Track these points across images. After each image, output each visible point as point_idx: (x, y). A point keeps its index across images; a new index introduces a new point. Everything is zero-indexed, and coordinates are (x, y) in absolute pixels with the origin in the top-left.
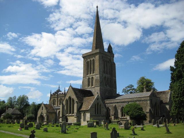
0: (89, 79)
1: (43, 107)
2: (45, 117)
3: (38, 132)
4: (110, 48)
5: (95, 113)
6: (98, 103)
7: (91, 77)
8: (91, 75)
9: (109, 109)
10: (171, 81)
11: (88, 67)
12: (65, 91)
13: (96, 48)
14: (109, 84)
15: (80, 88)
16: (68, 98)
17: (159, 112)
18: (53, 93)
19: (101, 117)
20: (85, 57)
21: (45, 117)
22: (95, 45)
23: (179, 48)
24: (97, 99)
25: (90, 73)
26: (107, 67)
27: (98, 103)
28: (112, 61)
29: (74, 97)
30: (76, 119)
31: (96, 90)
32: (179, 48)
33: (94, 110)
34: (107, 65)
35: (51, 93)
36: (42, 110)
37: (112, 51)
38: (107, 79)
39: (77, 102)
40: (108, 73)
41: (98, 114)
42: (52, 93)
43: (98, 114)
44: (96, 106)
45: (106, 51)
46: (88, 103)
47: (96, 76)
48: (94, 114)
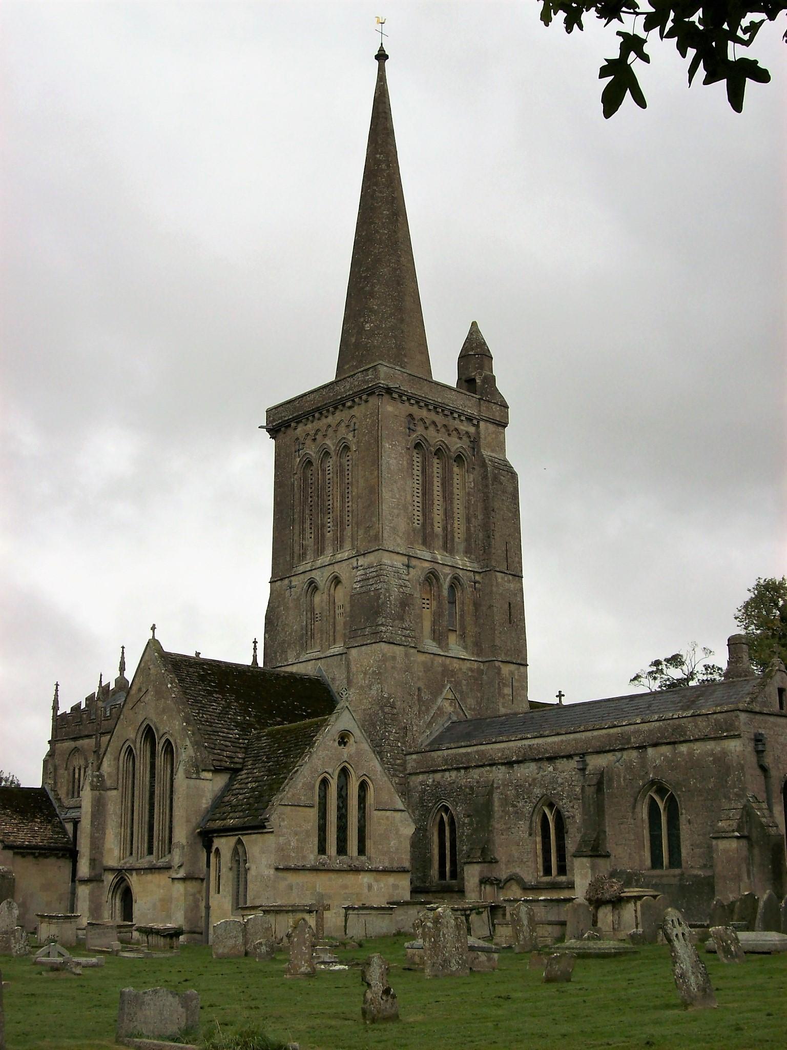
3: (782, 739)
4: (475, 355)
5: (322, 850)
6: (344, 772)
7: (327, 572)
8: (324, 559)
11: (304, 510)
12: (122, 668)
14: (463, 628)
15: (248, 662)
16: (132, 736)
17: (83, 960)
20: (283, 422)
25: (320, 551)
26: (448, 496)
27: (344, 772)
28: (486, 453)
38: (445, 593)
40: (462, 547)
41: (342, 849)
43: (342, 849)
45: (445, 369)
48: (312, 858)
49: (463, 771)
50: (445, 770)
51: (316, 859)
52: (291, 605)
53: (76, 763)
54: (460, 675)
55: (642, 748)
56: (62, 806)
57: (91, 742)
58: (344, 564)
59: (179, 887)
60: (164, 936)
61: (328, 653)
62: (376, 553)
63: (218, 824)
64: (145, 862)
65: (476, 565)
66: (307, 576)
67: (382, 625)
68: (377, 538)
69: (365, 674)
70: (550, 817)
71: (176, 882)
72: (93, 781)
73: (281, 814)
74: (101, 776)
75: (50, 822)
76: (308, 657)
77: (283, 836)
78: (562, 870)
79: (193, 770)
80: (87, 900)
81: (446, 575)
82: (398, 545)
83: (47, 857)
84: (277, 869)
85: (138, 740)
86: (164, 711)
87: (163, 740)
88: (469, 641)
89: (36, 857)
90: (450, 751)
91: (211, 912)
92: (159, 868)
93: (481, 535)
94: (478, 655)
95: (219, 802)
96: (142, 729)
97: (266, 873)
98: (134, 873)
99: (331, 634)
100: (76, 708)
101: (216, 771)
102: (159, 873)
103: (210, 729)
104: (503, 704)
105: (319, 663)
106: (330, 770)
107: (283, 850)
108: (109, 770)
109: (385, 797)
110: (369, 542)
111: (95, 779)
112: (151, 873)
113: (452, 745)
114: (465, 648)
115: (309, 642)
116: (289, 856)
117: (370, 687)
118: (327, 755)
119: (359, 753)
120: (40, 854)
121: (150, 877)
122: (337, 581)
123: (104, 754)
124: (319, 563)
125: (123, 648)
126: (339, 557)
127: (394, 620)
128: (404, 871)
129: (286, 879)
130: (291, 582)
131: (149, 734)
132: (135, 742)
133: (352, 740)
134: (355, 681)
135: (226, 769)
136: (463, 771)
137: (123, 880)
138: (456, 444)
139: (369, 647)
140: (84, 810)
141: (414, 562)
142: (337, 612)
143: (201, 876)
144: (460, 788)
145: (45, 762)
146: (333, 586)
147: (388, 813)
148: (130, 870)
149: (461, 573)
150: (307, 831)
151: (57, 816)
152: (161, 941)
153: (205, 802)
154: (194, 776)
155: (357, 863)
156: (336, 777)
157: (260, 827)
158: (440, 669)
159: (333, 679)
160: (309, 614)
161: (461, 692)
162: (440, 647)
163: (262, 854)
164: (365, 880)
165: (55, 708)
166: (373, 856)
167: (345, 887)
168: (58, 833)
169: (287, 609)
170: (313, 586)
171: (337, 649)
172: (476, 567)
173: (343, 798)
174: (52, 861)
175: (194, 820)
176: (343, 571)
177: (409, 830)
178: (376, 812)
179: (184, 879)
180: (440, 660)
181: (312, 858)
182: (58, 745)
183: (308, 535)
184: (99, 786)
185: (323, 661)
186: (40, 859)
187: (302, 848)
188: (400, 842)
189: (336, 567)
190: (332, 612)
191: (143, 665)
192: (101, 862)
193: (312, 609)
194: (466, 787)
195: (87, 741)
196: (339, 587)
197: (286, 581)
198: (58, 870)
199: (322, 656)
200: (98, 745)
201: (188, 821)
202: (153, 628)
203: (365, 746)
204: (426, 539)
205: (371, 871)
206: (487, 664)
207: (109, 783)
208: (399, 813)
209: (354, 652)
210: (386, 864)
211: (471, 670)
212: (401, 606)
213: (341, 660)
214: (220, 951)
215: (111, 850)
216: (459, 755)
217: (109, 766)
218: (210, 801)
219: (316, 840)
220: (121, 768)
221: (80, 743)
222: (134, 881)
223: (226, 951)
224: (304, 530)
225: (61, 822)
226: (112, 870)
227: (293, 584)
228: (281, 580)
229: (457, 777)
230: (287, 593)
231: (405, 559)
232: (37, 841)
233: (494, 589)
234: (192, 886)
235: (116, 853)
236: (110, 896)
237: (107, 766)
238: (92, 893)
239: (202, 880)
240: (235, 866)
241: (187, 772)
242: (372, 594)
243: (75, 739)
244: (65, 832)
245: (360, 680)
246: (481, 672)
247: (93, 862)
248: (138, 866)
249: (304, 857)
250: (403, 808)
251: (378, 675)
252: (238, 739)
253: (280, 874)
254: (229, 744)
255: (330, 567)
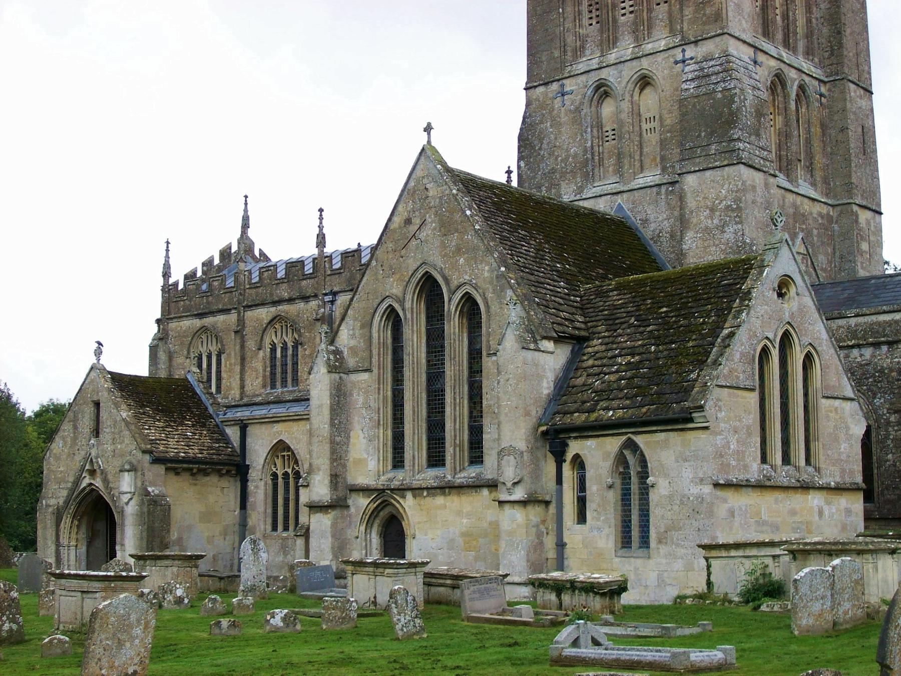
7: (629, 72)
14: (810, 157)
25: (609, 41)
27: (786, 341)
49: (885, 348)
50: (852, 347)
51: (761, 471)
52: (564, 119)
53: (204, 350)
54: (811, 222)
56: (216, 404)
57: (233, 317)
58: (660, 57)
59: (518, 515)
60: (603, 595)
61: (634, 184)
62: (718, 39)
63: (579, 418)
64: (430, 476)
65: (819, 71)
66: (593, 77)
67: (739, 139)
68: (718, 17)
69: (712, 210)
71: (507, 507)
72: (329, 359)
73: (719, 400)
74: (337, 352)
75: (204, 425)
76: (597, 191)
77: (720, 434)
79: (528, 337)
80: (329, 535)
81: (793, 80)
82: (744, 31)
83: (206, 474)
84: (716, 485)
85: (409, 297)
86: (458, 250)
87: (459, 295)
88: (818, 175)
89: (193, 475)
90: (860, 320)
91: (568, 551)
92: (461, 487)
93: (825, 30)
94: (827, 195)
95: (564, 386)
96: (415, 280)
97: (695, 490)
98: (409, 495)
99: (637, 157)
100: (190, 277)
101: (559, 340)
102: (459, 494)
103: (532, 278)
104: (862, 263)
105: (619, 199)
106: (771, 336)
107: (721, 456)
108: (353, 343)
109: (833, 380)
110: (704, 24)
111: (332, 357)
112: (444, 494)
113: (865, 311)
114: (813, 184)
115: (596, 170)
116: (729, 465)
117: (722, 228)
118: (766, 312)
119: (801, 309)
120: (199, 470)
121: (440, 500)
122: (645, 82)
123: (343, 319)
124: (612, 57)
125: (246, 197)
126: (612, 57)
127: (750, 135)
128: (858, 489)
129: (725, 501)
130: (563, 86)
131: (430, 289)
132: (402, 302)
133: (793, 290)
134: (694, 220)
135: (572, 337)
136: (885, 348)
137: (385, 504)
139: (718, 172)
140: (314, 402)
141: (761, 58)
142: (645, 126)
143: (547, 498)
144: (882, 371)
145: (153, 349)
146: (637, 89)
147: (837, 403)
148: (402, 490)
149: (807, 79)
150: (748, 427)
151: (211, 417)
152: (596, 603)
153: (547, 387)
154: (532, 346)
155: (805, 477)
156: (777, 346)
157: (681, 420)
158: (791, 211)
159: (645, 221)
160: (595, 131)
161: (813, 246)
163: (676, 464)
164: (816, 502)
165: (166, 274)
166: (822, 466)
167: (793, 513)
168: (218, 441)
169: (556, 124)
170: (602, 91)
171: (651, 176)
172: (818, 73)
174: (213, 479)
175: (534, 413)
176: (659, 68)
177: (859, 430)
178: (824, 401)
179: (524, 503)
180: (790, 197)
181: (754, 470)
182: (173, 325)
183: (585, 22)
184: (338, 366)
185: (625, 195)
186: (199, 477)
187: (743, 452)
188: (851, 446)
189: (645, 63)
190: (637, 128)
191: (412, 184)
192: (345, 479)
193: (599, 125)
194: (891, 370)
195: (221, 318)
196: (647, 90)
197: (555, 86)
198: (221, 494)
199: (626, 188)
200: (241, 322)
201: (528, 414)
202: (428, 129)
203: (808, 301)
205: (821, 488)
206: (839, 208)
207: (351, 362)
208: (849, 403)
209: (691, 181)
210: (838, 479)
211: (820, 214)
212: (756, 116)
213: (658, 193)
214: (804, 622)
215: (359, 462)
216: (879, 324)
217: (353, 336)
218: (552, 384)
219: (759, 439)
220: (375, 340)
221: (209, 321)
222: (409, 505)
223: (811, 621)
224: (580, 13)
225: (217, 426)
226: (365, 490)
227: (567, 89)
228: (546, 84)
229: (873, 356)
230: (557, 103)
231: (751, 51)
232: (194, 452)
233: (849, 105)
234: (534, 513)
235: (372, 465)
236: (363, 528)
237: (345, 338)
238: (334, 525)
239: (547, 503)
240: (618, 482)
241: (521, 339)
242: (719, 95)
243: (201, 316)
244: (226, 440)
245: (702, 218)
246: (830, 219)
247: (335, 479)
248: (416, 484)
249: (746, 467)
250: (852, 396)
251: (736, 211)
252: (568, 295)
253: (720, 493)
254: (561, 301)
255: (635, 63)
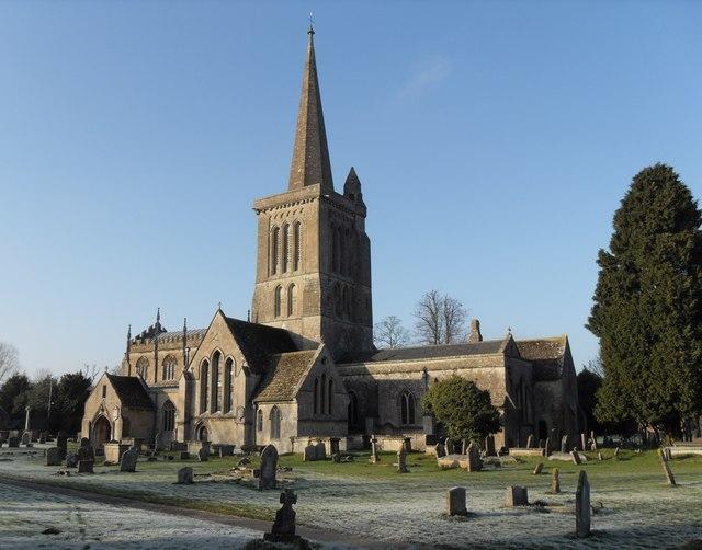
0: (278, 289)
1: (105, 387)
2: (117, 422)
6: (324, 376)
9: (278, 411)
10: (594, 299)
13: (307, 182)
18: (138, 338)
19: (331, 425)
21: (117, 422)
22: (301, 170)
23: (677, 176)
24: (322, 360)
27: (324, 376)
29: (232, 350)
30: (242, 428)
31: (307, 325)
32: (677, 176)
33: (311, 400)
34: (342, 243)
35: (129, 337)
36: (104, 395)
37: (360, 195)
39: (244, 368)
42: (133, 337)
43: (323, 412)
44: (316, 384)
45: (339, 188)
46: (293, 374)
47: (305, 277)
55: (456, 369)
70: (407, 399)
78: (412, 421)
138: (347, 225)
162: (499, 347)
173: (323, 385)
204: (334, 270)
